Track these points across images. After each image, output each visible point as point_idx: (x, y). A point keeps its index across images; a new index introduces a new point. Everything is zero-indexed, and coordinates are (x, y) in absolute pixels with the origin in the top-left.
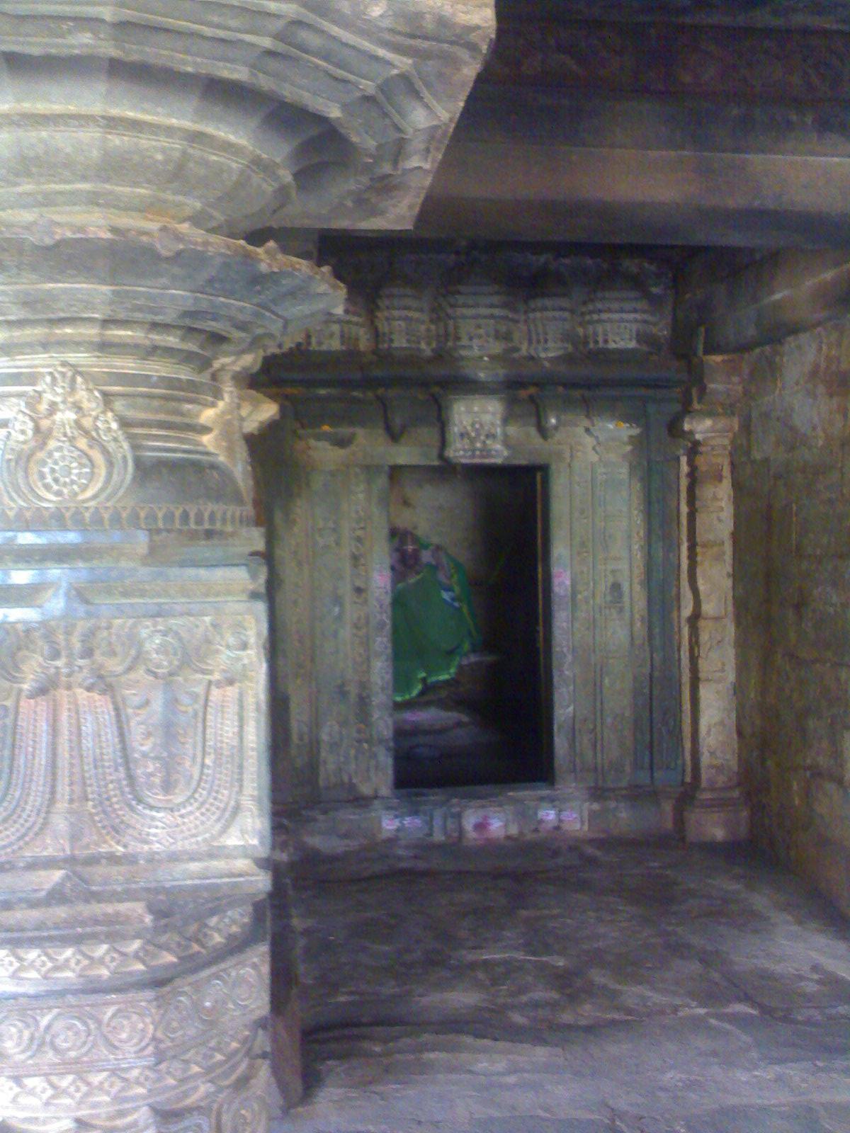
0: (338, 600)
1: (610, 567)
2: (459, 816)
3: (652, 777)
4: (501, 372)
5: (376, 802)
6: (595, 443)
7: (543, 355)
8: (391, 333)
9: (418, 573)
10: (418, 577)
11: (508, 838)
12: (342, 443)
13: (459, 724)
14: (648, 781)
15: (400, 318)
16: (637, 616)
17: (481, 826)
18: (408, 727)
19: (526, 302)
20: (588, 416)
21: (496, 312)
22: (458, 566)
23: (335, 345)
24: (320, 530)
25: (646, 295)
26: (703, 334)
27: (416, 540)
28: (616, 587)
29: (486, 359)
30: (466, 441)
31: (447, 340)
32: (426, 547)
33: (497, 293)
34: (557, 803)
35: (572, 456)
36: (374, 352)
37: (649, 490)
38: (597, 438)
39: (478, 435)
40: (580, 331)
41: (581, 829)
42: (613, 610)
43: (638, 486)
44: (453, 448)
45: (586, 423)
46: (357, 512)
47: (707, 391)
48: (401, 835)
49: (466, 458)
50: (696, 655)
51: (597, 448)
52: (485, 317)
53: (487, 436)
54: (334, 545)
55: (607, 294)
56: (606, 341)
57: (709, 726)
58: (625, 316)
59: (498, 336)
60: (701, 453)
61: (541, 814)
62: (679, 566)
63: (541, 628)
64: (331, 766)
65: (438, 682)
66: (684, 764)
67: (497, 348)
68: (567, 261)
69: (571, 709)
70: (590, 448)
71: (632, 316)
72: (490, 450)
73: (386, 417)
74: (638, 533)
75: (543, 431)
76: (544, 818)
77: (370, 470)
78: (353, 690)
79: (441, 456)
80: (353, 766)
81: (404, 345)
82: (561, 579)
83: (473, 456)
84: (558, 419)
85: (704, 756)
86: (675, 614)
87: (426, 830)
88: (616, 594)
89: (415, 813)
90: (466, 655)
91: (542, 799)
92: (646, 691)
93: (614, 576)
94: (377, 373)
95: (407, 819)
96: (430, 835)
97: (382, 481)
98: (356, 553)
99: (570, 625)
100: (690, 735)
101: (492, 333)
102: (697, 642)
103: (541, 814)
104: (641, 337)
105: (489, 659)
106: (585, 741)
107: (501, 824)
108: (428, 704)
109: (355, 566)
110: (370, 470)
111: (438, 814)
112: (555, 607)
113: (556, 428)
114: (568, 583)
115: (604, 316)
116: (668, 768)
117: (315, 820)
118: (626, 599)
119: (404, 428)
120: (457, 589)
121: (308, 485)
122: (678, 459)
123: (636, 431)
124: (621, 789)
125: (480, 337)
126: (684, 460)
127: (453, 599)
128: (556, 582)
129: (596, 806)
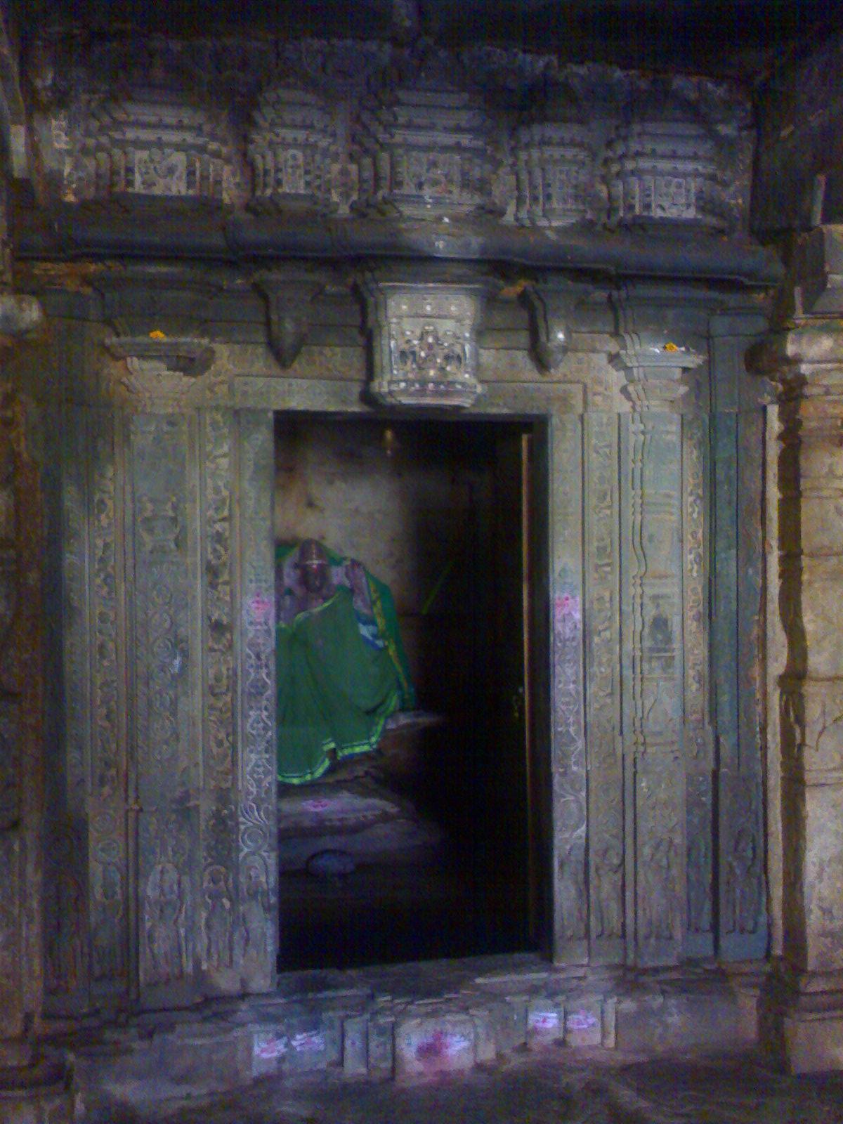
0: (179, 645)
1: (649, 591)
2: (392, 1032)
3: (716, 947)
4: (475, 242)
5: (244, 1006)
6: (624, 382)
7: (543, 223)
8: (278, 170)
9: (325, 599)
10: (326, 605)
11: (479, 1067)
12: (189, 365)
13: (385, 818)
14: (709, 951)
15: (295, 144)
16: (691, 673)
17: (431, 1051)
18: (307, 823)
19: (513, 132)
20: (616, 334)
21: (465, 140)
22: (382, 590)
23: (178, 187)
24: (146, 520)
25: (712, 135)
26: (823, 187)
27: (322, 552)
28: (660, 624)
29: (446, 220)
30: (410, 365)
31: (377, 187)
32: (338, 563)
33: (467, 107)
34: (560, 998)
35: (585, 402)
36: (247, 208)
37: (714, 464)
38: (628, 369)
39: (431, 356)
40: (603, 190)
41: (602, 1043)
42: (655, 664)
43: (693, 456)
44: (387, 377)
45: (612, 346)
46: (217, 490)
47: (829, 286)
48: (286, 1067)
49: (411, 395)
50: (798, 741)
51: (631, 389)
52: (444, 149)
53: (447, 358)
54: (172, 546)
55: (651, 127)
56: (647, 206)
57: (821, 865)
58: (681, 166)
59: (466, 184)
60: (807, 397)
61: (534, 1019)
62: (764, 588)
63: (526, 690)
64: (161, 947)
65: (352, 756)
66: (770, 925)
67: (467, 202)
68: (582, 70)
69: (582, 830)
70: (616, 390)
71: (690, 166)
72: (452, 383)
73: (268, 323)
74: (694, 534)
75: (541, 359)
76: (540, 1025)
77: (240, 417)
78: (206, 806)
79: (367, 397)
80: (202, 945)
81: (302, 192)
82: (566, 611)
83: (422, 392)
84: (568, 333)
85: (812, 917)
86: (756, 671)
87: (334, 1055)
88: (660, 637)
89: (313, 1026)
90: (392, 716)
91: (534, 991)
92: (707, 799)
93: (658, 606)
94: (252, 234)
95: (298, 1037)
96: (340, 1063)
97: (262, 439)
98: (214, 562)
99: (581, 689)
100: (781, 875)
101: (457, 177)
102: (800, 720)
103: (534, 1019)
104: (705, 204)
105: (425, 720)
106: (605, 887)
107: (465, 1044)
108: (339, 786)
109: (213, 586)
110: (240, 417)
111: (354, 1029)
112: (555, 658)
113: (565, 349)
114: (578, 616)
115: (645, 164)
116: (742, 930)
117: (129, 1051)
118: (676, 645)
119: (302, 341)
120: (380, 621)
121: (127, 439)
122: (764, 409)
123: (694, 360)
124: (668, 969)
125: (435, 183)
126: (773, 411)
127: (375, 636)
128: (557, 614)
129: (629, 1005)
